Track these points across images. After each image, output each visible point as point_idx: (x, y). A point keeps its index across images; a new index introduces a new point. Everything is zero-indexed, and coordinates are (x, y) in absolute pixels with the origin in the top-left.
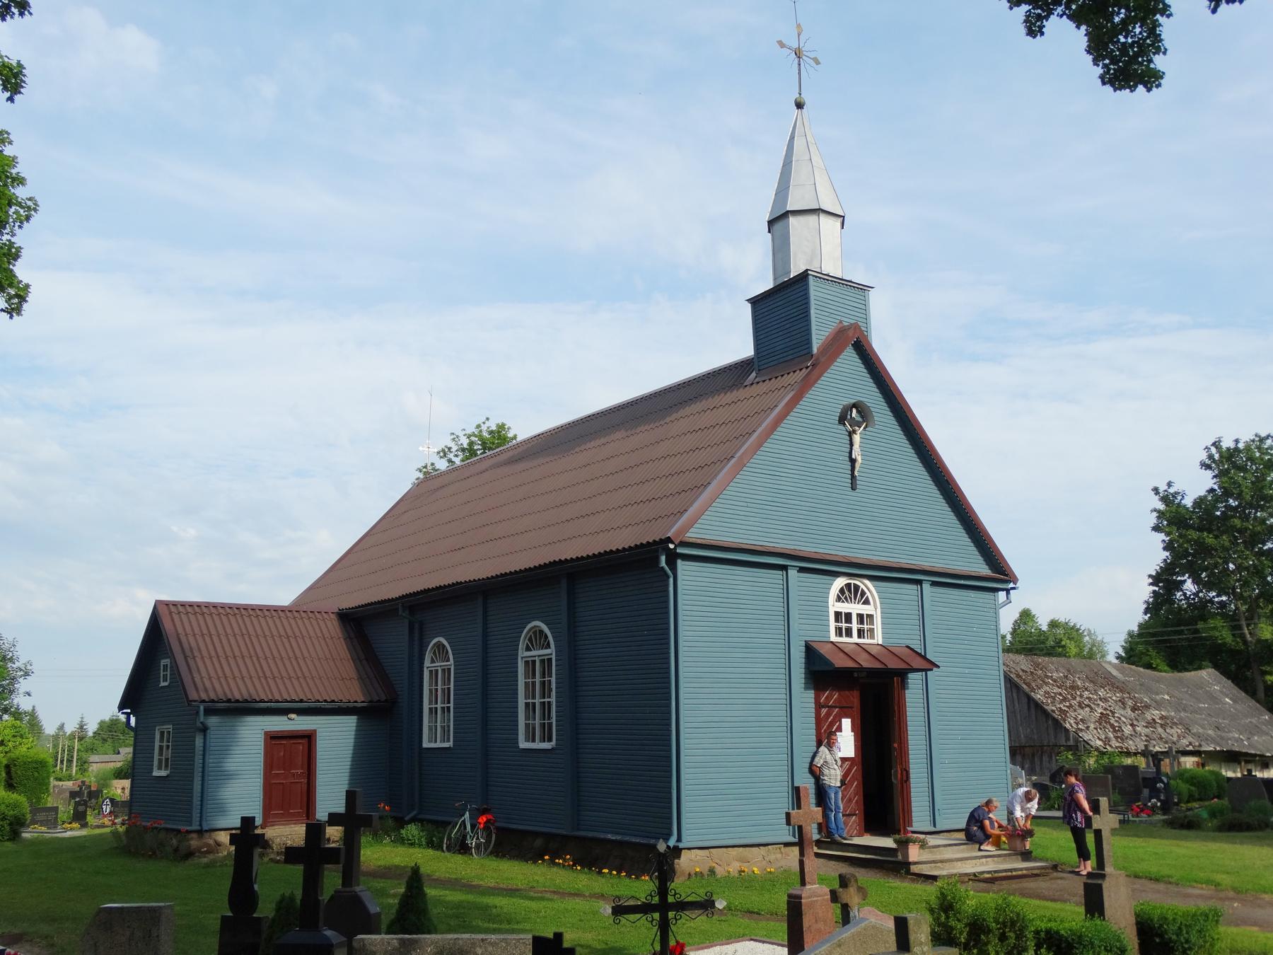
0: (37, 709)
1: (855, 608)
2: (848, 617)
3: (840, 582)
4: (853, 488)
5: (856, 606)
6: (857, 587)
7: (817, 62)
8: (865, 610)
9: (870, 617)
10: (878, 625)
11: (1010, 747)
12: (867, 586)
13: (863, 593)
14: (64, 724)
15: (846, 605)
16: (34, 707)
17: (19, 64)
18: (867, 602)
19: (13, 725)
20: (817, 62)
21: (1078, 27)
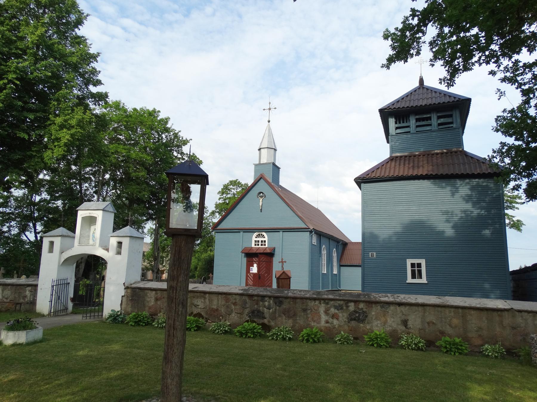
0: (520, 233)
1: (260, 239)
2: (258, 241)
3: (256, 234)
4: (261, 212)
5: (260, 239)
6: (262, 234)
7: (191, 140)
8: (263, 239)
9: (265, 241)
10: (266, 243)
11: (515, 299)
12: (264, 234)
13: (263, 235)
14: (108, 252)
15: (258, 238)
16: (530, 55)
17: (112, 310)
18: (264, 237)
19: (31, 355)
20: (191, 140)
21: (410, 11)
